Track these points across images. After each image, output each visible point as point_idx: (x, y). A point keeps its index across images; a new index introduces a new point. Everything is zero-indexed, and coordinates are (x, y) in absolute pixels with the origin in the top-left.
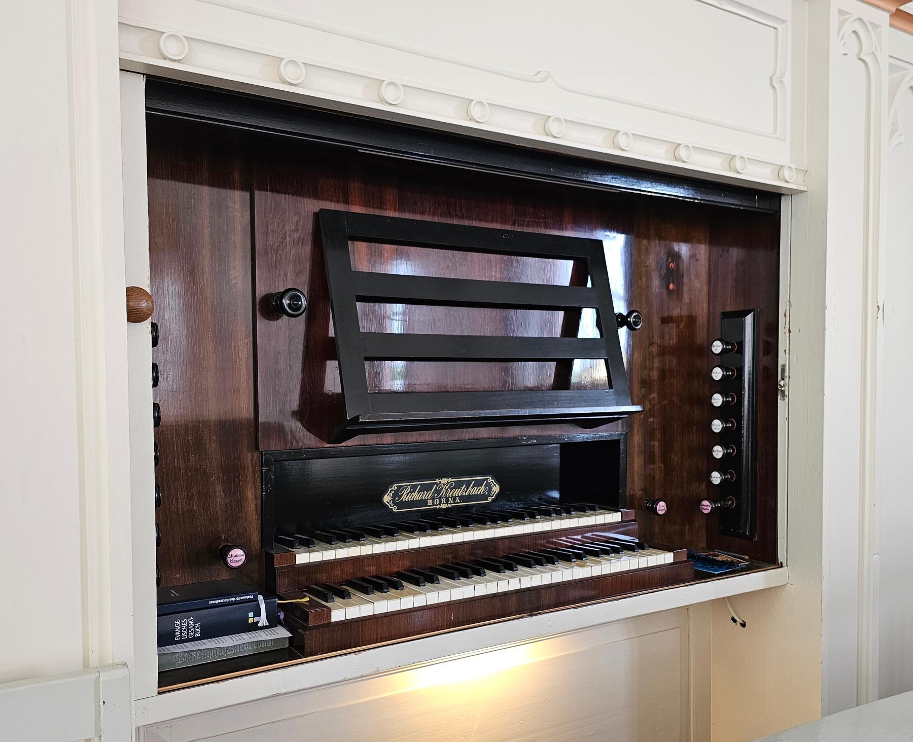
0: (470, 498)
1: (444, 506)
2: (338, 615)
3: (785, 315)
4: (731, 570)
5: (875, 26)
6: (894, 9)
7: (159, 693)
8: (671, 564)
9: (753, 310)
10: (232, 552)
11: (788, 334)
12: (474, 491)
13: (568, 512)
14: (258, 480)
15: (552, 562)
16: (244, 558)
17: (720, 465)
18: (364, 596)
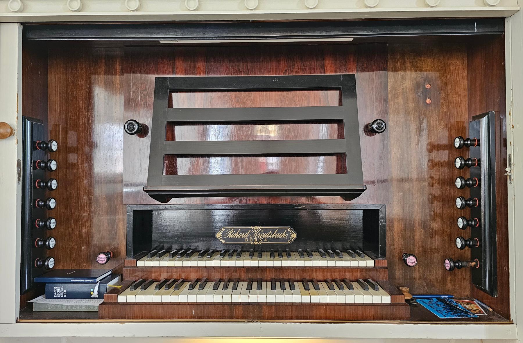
0: (275, 239)
1: (256, 243)
3: (510, 114)
9: (487, 114)
10: (99, 256)
11: (512, 129)
12: (278, 236)
17: (459, 233)
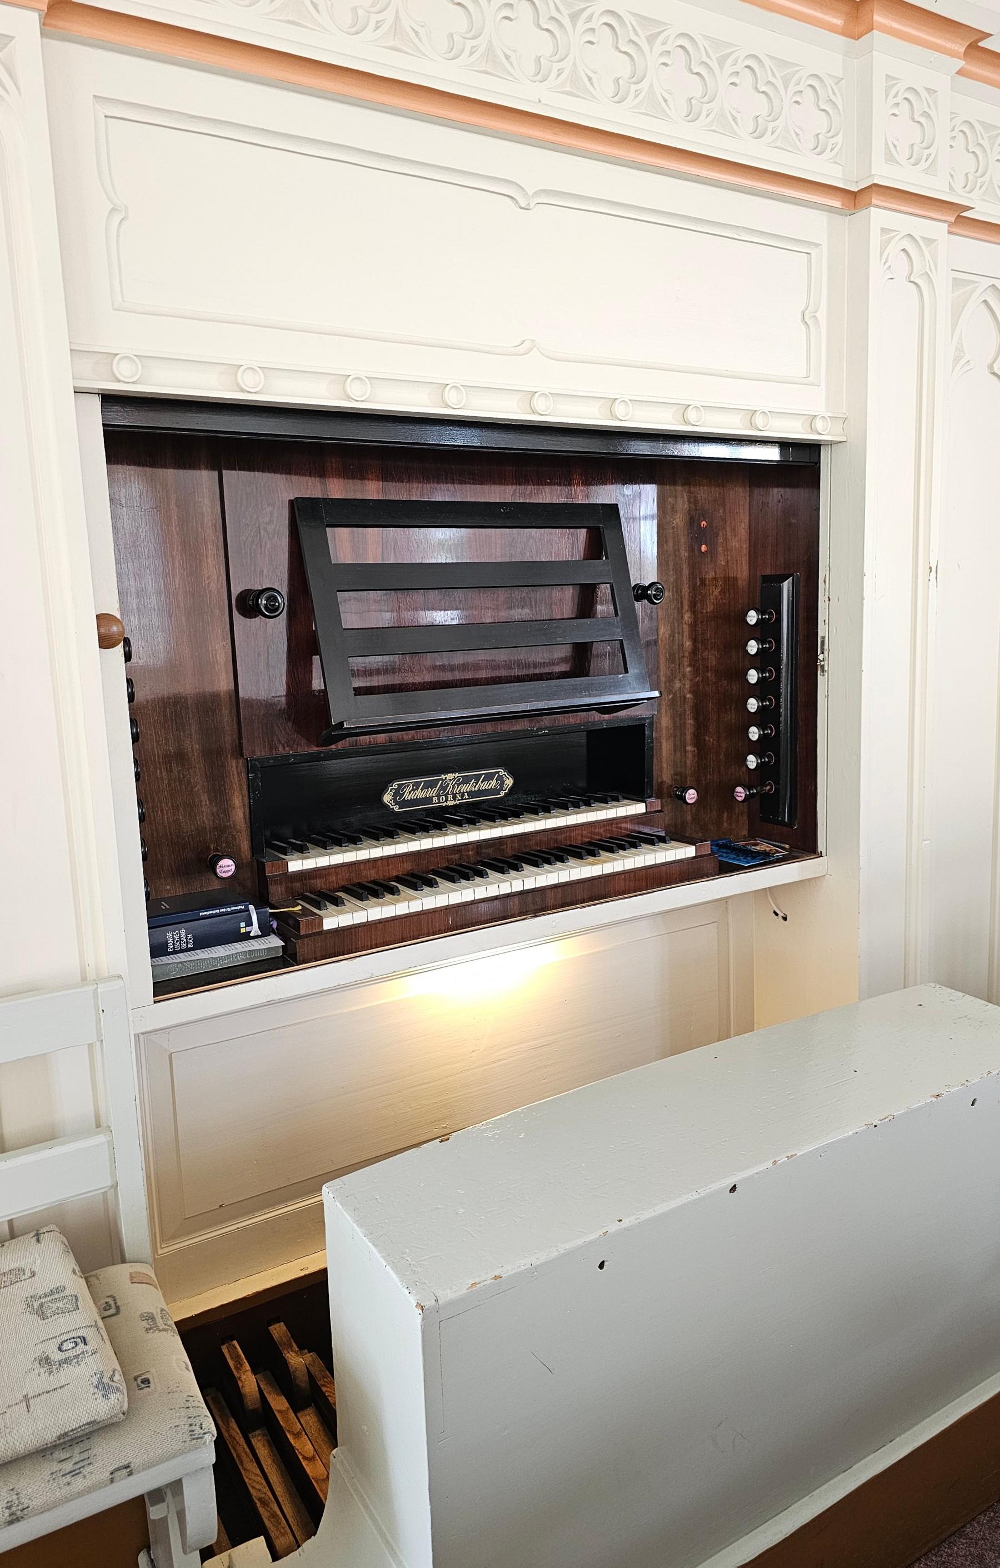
0: (480, 793)
1: (451, 803)
2: (330, 923)
4: (766, 860)
5: (929, 241)
6: (953, 220)
7: (155, 1002)
8: (693, 858)
10: (220, 863)
11: (827, 602)
12: (484, 786)
13: (588, 804)
14: (245, 787)
15: (634, 846)
16: (233, 868)
17: (756, 748)
18: (359, 903)
